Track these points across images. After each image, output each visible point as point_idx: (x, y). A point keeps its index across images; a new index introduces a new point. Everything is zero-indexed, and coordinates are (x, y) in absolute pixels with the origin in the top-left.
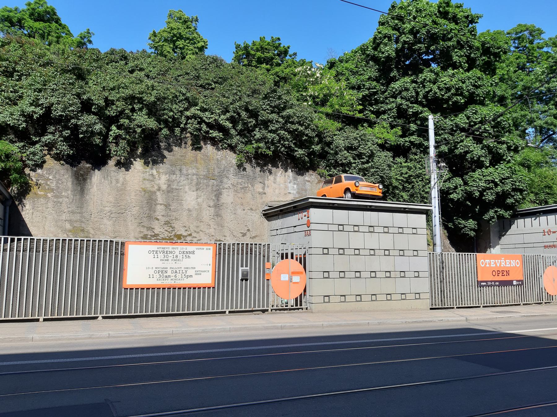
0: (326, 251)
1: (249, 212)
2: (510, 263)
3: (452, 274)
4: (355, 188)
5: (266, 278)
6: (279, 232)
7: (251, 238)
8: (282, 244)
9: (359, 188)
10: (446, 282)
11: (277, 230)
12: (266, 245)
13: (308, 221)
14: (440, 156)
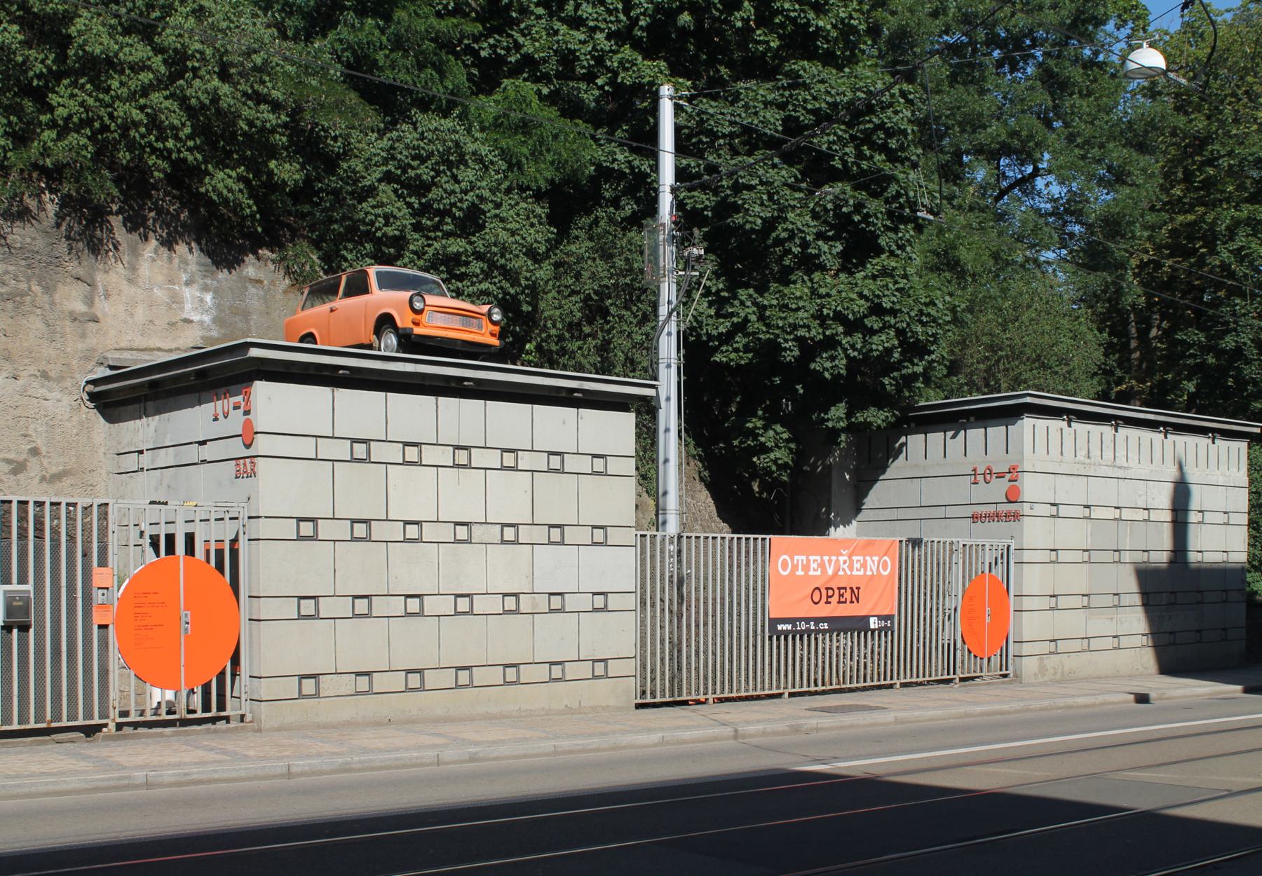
0: (307, 529)
1: (35, 384)
2: (864, 565)
3: (706, 598)
4: (412, 316)
5: (97, 619)
6: (146, 460)
7: (43, 479)
8: (151, 503)
9: (424, 318)
10: (689, 626)
11: (141, 452)
12: (95, 508)
13: (248, 425)
14: (687, 218)
